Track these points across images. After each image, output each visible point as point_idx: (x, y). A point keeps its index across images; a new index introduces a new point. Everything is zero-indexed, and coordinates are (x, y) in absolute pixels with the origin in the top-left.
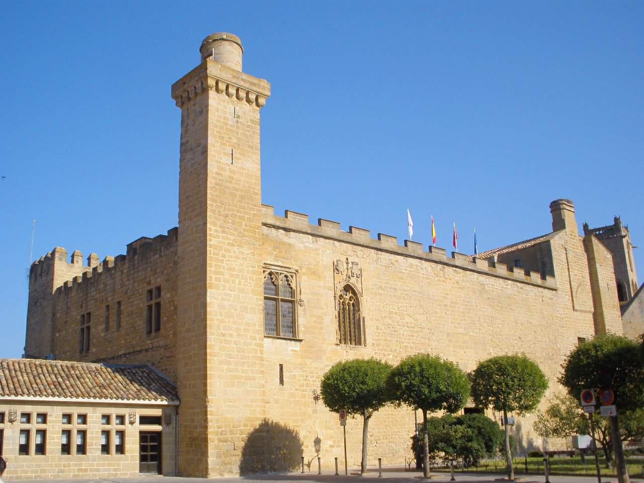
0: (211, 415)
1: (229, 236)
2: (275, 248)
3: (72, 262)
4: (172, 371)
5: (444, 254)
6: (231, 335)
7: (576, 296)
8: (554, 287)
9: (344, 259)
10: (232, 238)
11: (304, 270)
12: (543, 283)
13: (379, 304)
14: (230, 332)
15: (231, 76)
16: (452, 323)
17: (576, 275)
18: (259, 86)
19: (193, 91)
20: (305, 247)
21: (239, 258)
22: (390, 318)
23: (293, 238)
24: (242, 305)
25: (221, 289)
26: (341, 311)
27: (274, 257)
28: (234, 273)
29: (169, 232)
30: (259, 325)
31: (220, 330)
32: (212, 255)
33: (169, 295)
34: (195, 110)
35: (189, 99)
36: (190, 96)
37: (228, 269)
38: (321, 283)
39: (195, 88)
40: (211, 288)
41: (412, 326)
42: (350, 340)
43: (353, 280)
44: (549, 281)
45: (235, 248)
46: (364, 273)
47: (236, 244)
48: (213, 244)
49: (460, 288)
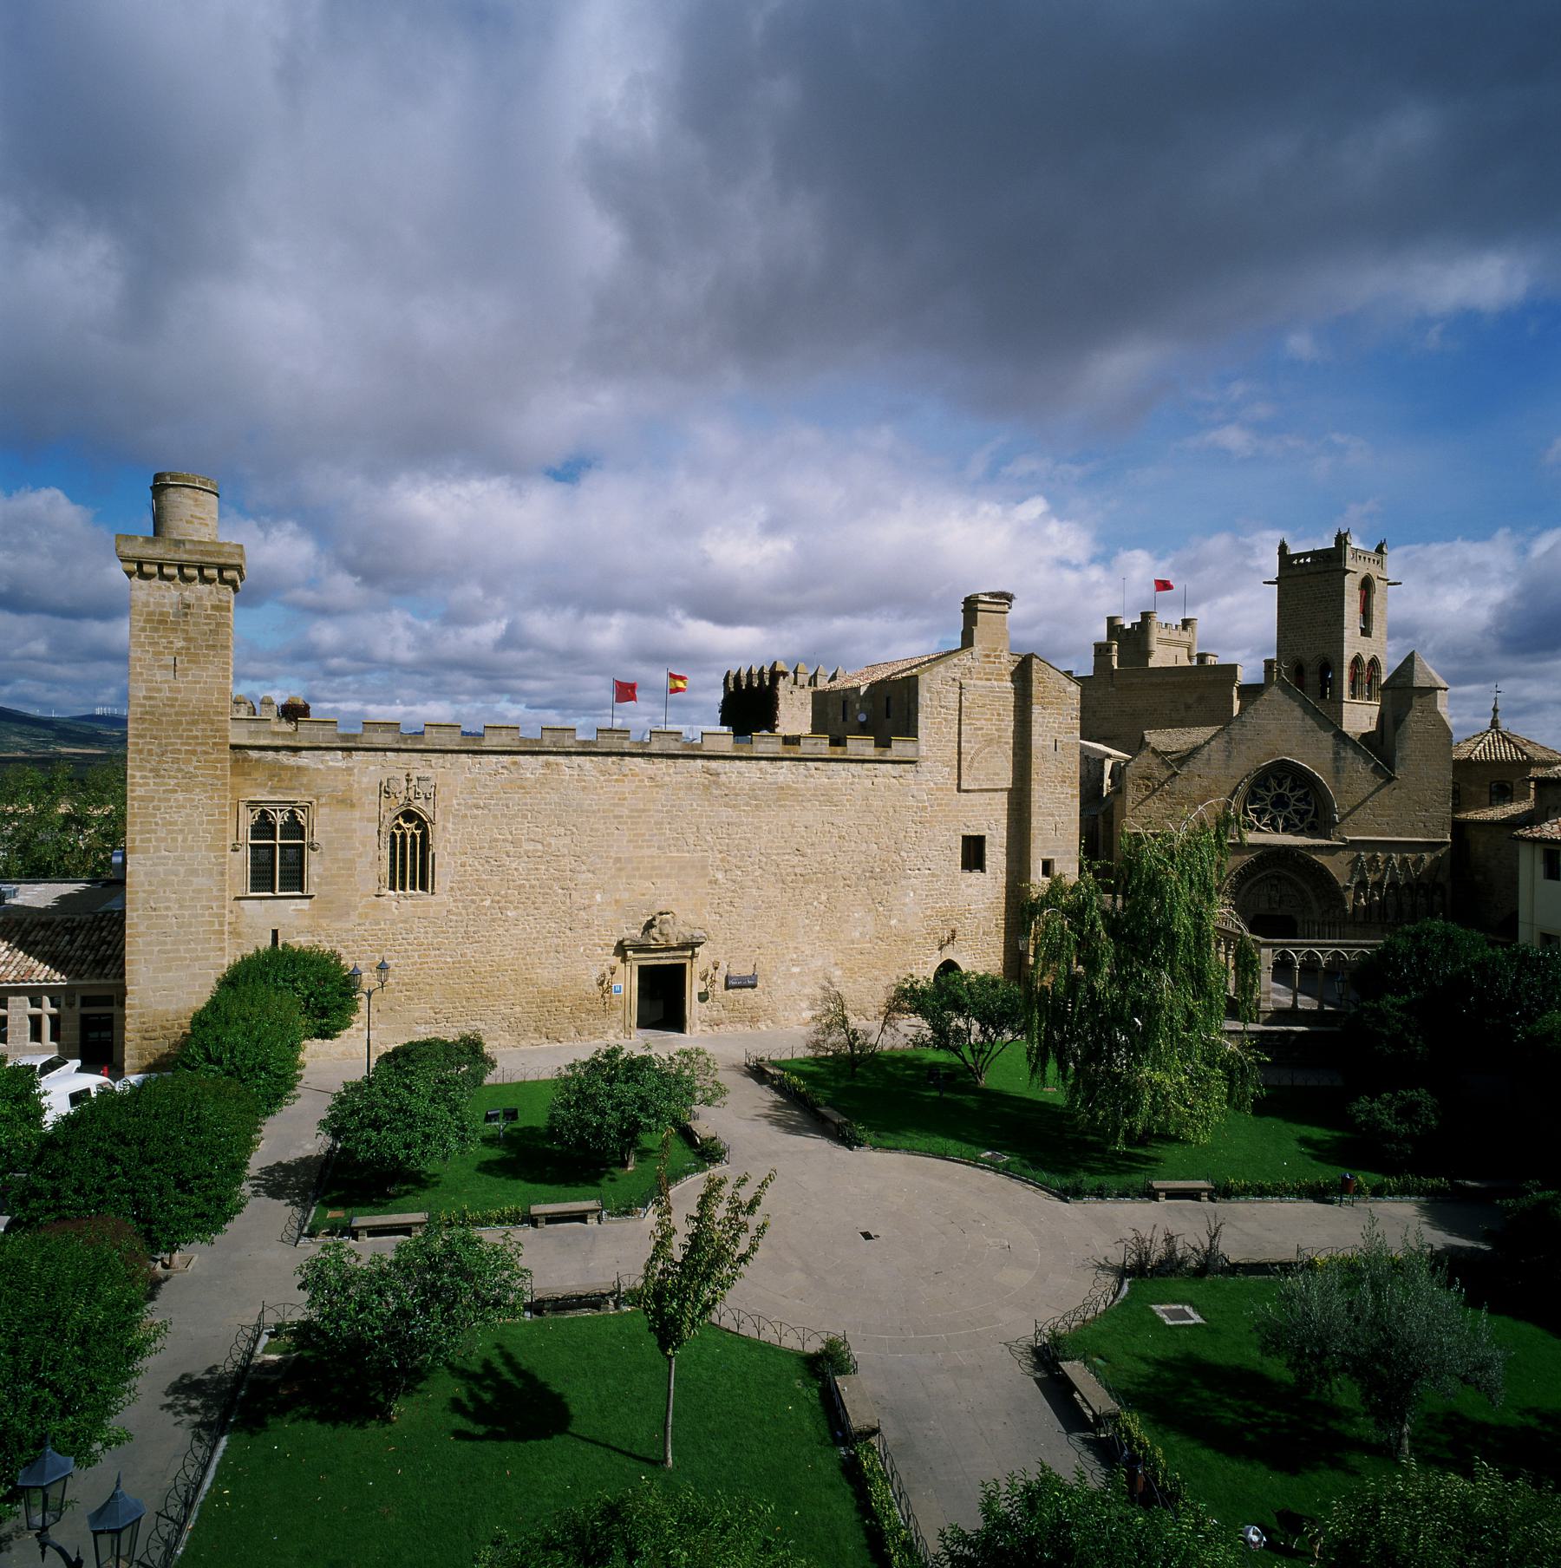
11: (323, 800)
20: (329, 768)
23: (305, 759)
38: (357, 814)
43: (418, 805)
44: (899, 748)
45: (180, 796)
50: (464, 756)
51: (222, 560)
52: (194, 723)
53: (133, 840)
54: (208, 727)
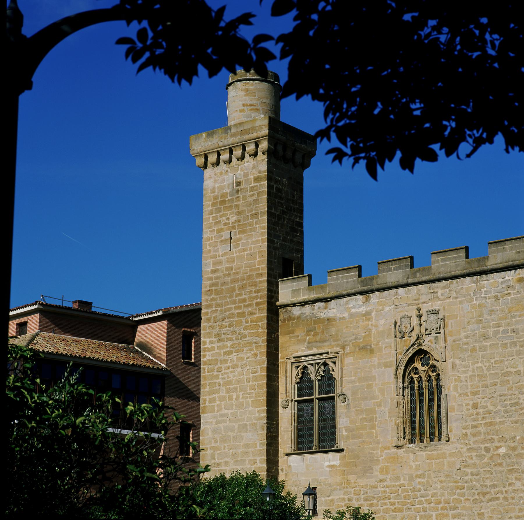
10: (229, 344)
11: (348, 349)
13: (480, 365)
20: (352, 315)
21: (236, 366)
22: (503, 383)
23: (334, 309)
24: (241, 423)
25: (216, 411)
27: (306, 344)
28: (232, 387)
31: (215, 459)
37: (225, 384)
38: (375, 360)
40: (204, 413)
43: (427, 344)
45: (233, 357)
46: (450, 322)
48: (208, 360)
50: (468, 279)
51: (254, 135)
52: (243, 288)
54: (253, 289)
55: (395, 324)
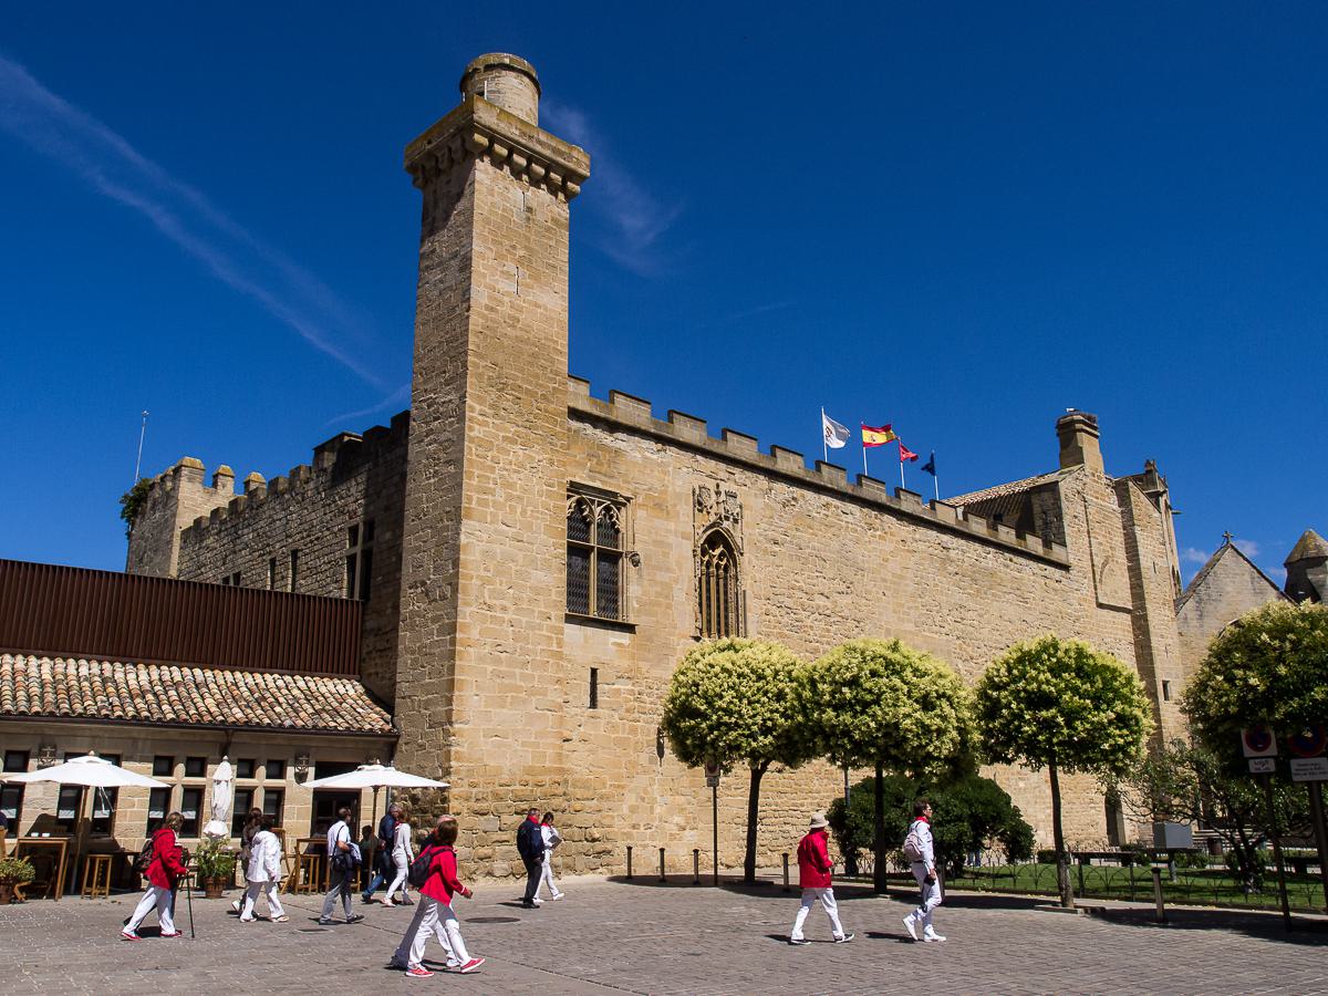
0: (458, 760)
1: (508, 425)
2: (590, 456)
3: (215, 485)
4: (387, 676)
5: (881, 490)
6: (504, 609)
7: (1101, 580)
8: (1063, 560)
9: (711, 484)
12: (1045, 553)
14: (504, 602)
15: (517, 133)
16: (894, 612)
17: (1101, 544)
18: (570, 157)
19: (446, 156)
23: (621, 441)
25: (489, 520)
26: (704, 578)
29: (394, 420)
30: (558, 592)
32: (474, 457)
33: (388, 535)
34: (449, 192)
35: (439, 172)
36: (442, 166)
38: (672, 526)
39: (450, 149)
40: (469, 517)
41: (828, 612)
42: (719, 631)
44: (1057, 553)
47: (519, 441)
49: (908, 551)
53: (470, 499)
55: (694, 492)
